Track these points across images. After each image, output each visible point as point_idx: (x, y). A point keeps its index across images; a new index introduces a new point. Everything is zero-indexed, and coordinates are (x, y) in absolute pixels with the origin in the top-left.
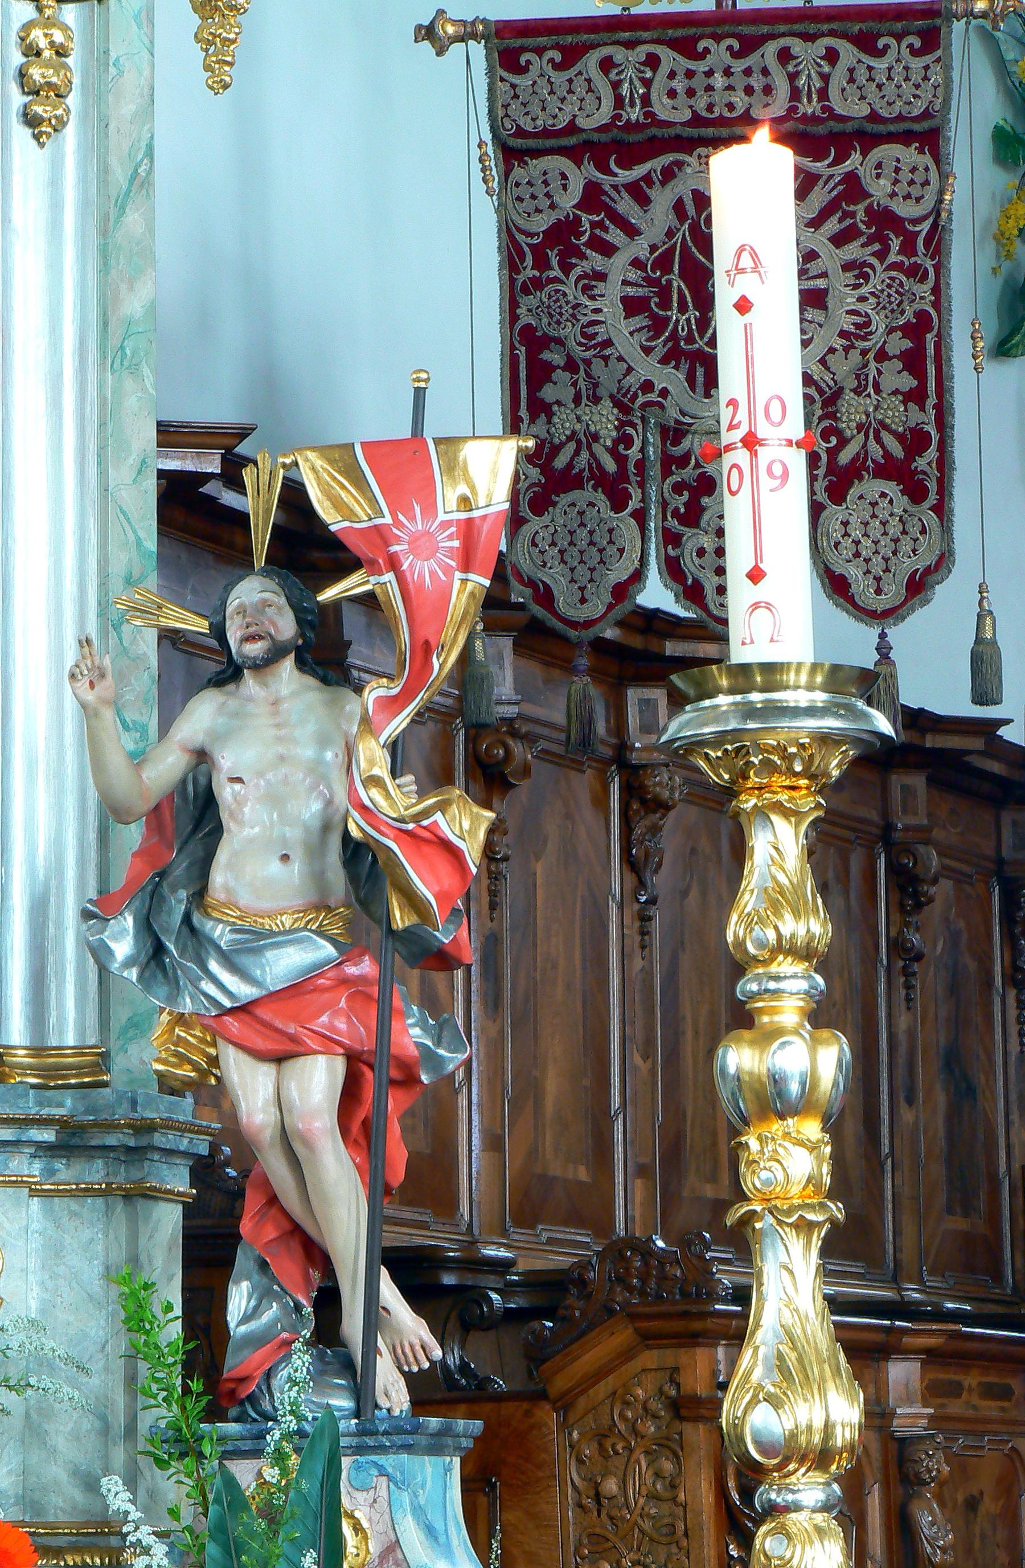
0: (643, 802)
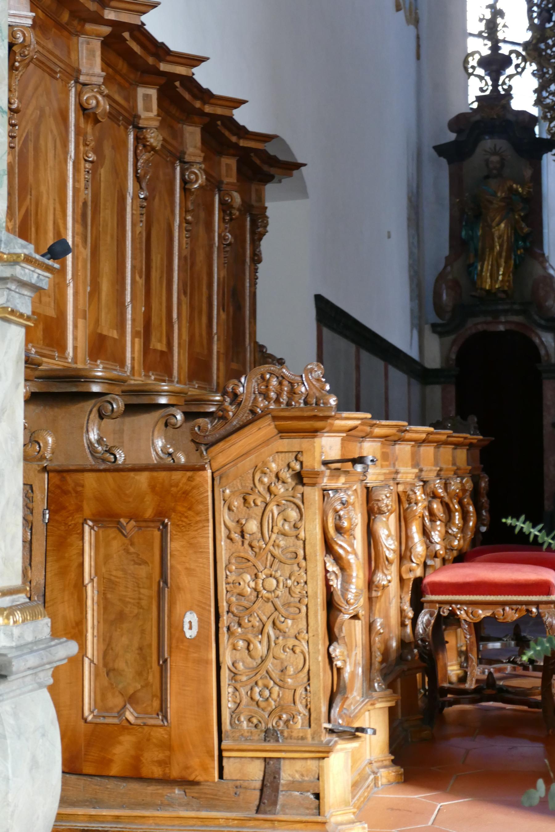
0: (145, 146)
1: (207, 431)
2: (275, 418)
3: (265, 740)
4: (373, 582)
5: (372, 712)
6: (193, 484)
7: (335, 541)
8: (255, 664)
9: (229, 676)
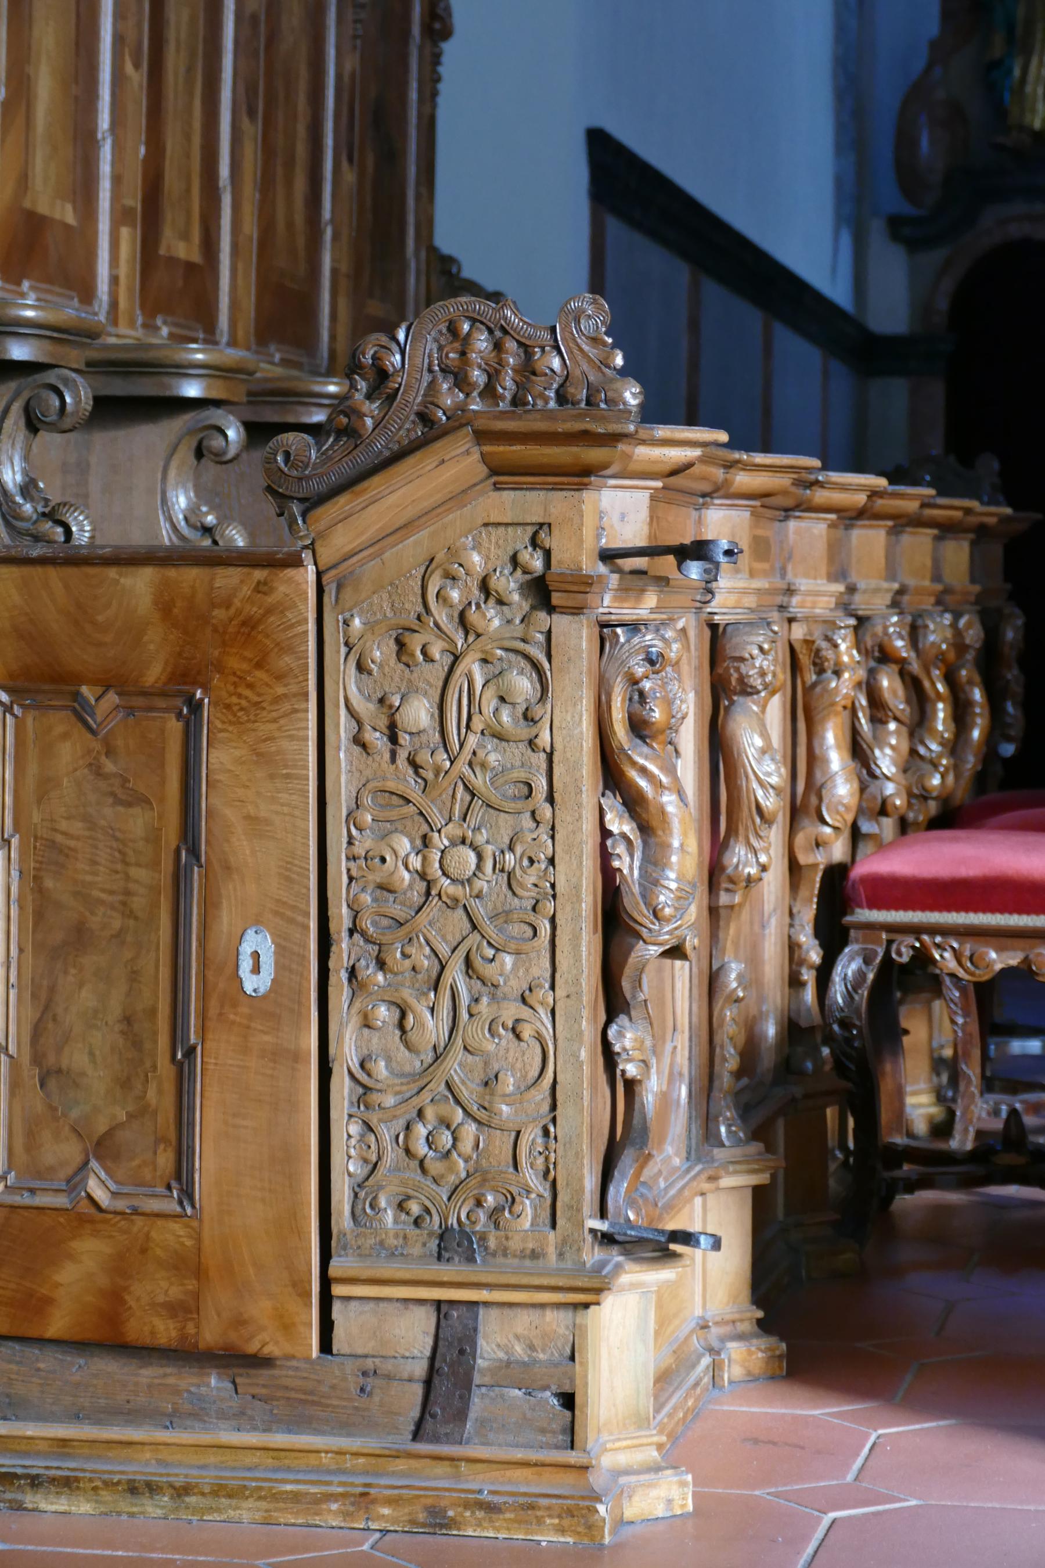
1: (307, 466)
2: (482, 436)
3: (439, 1258)
4: (723, 869)
5: (710, 1197)
6: (270, 600)
7: (630, 758)
8: (418, 1064)
9: (351, 1090)
